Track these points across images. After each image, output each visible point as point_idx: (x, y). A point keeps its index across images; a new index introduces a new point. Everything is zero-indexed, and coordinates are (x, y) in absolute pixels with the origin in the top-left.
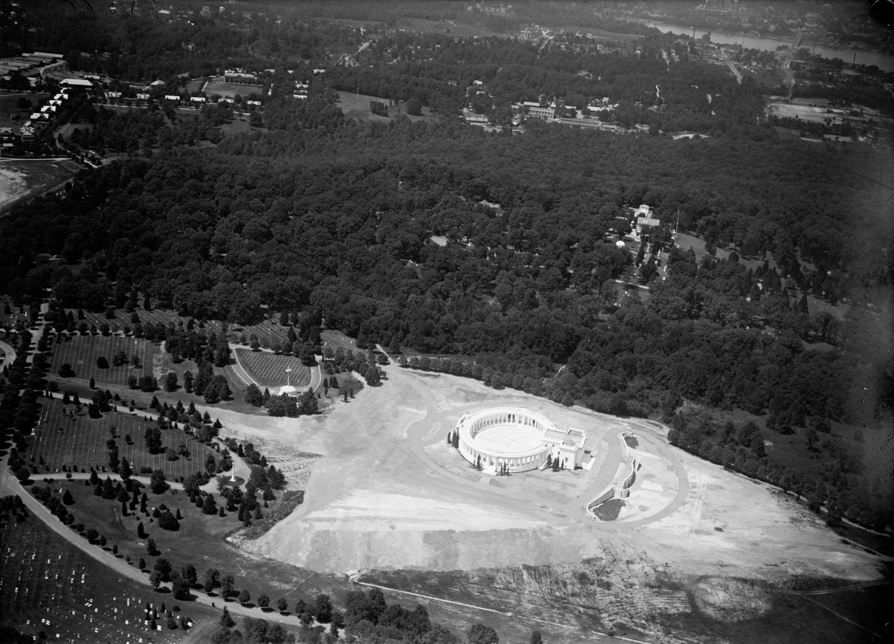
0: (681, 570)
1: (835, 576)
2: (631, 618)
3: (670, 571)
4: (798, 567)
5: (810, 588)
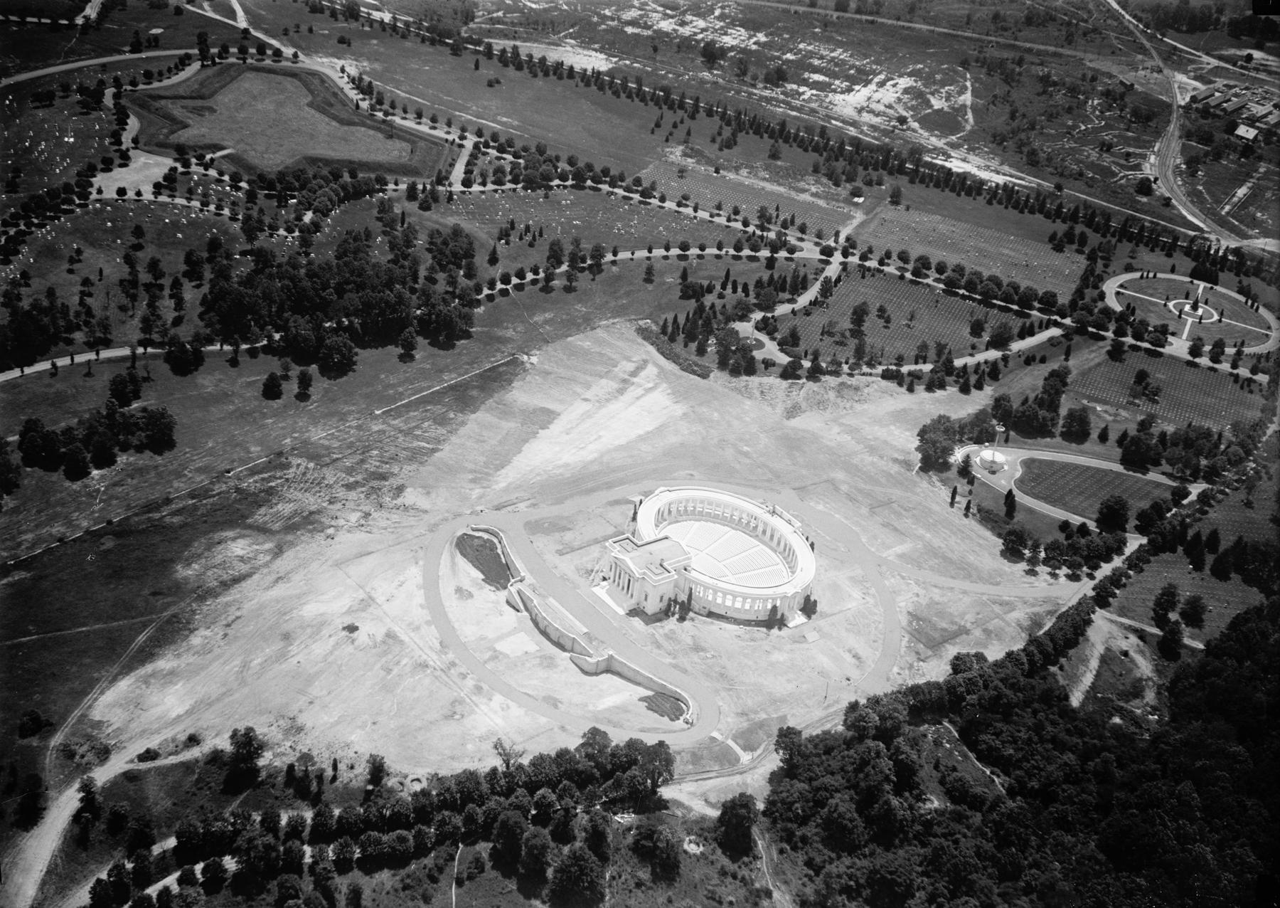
0: (306, 548)
1: (149, 668)
2: (287, 480)
3: (320, 537)
4: (204, 646)
5: (160, 629)
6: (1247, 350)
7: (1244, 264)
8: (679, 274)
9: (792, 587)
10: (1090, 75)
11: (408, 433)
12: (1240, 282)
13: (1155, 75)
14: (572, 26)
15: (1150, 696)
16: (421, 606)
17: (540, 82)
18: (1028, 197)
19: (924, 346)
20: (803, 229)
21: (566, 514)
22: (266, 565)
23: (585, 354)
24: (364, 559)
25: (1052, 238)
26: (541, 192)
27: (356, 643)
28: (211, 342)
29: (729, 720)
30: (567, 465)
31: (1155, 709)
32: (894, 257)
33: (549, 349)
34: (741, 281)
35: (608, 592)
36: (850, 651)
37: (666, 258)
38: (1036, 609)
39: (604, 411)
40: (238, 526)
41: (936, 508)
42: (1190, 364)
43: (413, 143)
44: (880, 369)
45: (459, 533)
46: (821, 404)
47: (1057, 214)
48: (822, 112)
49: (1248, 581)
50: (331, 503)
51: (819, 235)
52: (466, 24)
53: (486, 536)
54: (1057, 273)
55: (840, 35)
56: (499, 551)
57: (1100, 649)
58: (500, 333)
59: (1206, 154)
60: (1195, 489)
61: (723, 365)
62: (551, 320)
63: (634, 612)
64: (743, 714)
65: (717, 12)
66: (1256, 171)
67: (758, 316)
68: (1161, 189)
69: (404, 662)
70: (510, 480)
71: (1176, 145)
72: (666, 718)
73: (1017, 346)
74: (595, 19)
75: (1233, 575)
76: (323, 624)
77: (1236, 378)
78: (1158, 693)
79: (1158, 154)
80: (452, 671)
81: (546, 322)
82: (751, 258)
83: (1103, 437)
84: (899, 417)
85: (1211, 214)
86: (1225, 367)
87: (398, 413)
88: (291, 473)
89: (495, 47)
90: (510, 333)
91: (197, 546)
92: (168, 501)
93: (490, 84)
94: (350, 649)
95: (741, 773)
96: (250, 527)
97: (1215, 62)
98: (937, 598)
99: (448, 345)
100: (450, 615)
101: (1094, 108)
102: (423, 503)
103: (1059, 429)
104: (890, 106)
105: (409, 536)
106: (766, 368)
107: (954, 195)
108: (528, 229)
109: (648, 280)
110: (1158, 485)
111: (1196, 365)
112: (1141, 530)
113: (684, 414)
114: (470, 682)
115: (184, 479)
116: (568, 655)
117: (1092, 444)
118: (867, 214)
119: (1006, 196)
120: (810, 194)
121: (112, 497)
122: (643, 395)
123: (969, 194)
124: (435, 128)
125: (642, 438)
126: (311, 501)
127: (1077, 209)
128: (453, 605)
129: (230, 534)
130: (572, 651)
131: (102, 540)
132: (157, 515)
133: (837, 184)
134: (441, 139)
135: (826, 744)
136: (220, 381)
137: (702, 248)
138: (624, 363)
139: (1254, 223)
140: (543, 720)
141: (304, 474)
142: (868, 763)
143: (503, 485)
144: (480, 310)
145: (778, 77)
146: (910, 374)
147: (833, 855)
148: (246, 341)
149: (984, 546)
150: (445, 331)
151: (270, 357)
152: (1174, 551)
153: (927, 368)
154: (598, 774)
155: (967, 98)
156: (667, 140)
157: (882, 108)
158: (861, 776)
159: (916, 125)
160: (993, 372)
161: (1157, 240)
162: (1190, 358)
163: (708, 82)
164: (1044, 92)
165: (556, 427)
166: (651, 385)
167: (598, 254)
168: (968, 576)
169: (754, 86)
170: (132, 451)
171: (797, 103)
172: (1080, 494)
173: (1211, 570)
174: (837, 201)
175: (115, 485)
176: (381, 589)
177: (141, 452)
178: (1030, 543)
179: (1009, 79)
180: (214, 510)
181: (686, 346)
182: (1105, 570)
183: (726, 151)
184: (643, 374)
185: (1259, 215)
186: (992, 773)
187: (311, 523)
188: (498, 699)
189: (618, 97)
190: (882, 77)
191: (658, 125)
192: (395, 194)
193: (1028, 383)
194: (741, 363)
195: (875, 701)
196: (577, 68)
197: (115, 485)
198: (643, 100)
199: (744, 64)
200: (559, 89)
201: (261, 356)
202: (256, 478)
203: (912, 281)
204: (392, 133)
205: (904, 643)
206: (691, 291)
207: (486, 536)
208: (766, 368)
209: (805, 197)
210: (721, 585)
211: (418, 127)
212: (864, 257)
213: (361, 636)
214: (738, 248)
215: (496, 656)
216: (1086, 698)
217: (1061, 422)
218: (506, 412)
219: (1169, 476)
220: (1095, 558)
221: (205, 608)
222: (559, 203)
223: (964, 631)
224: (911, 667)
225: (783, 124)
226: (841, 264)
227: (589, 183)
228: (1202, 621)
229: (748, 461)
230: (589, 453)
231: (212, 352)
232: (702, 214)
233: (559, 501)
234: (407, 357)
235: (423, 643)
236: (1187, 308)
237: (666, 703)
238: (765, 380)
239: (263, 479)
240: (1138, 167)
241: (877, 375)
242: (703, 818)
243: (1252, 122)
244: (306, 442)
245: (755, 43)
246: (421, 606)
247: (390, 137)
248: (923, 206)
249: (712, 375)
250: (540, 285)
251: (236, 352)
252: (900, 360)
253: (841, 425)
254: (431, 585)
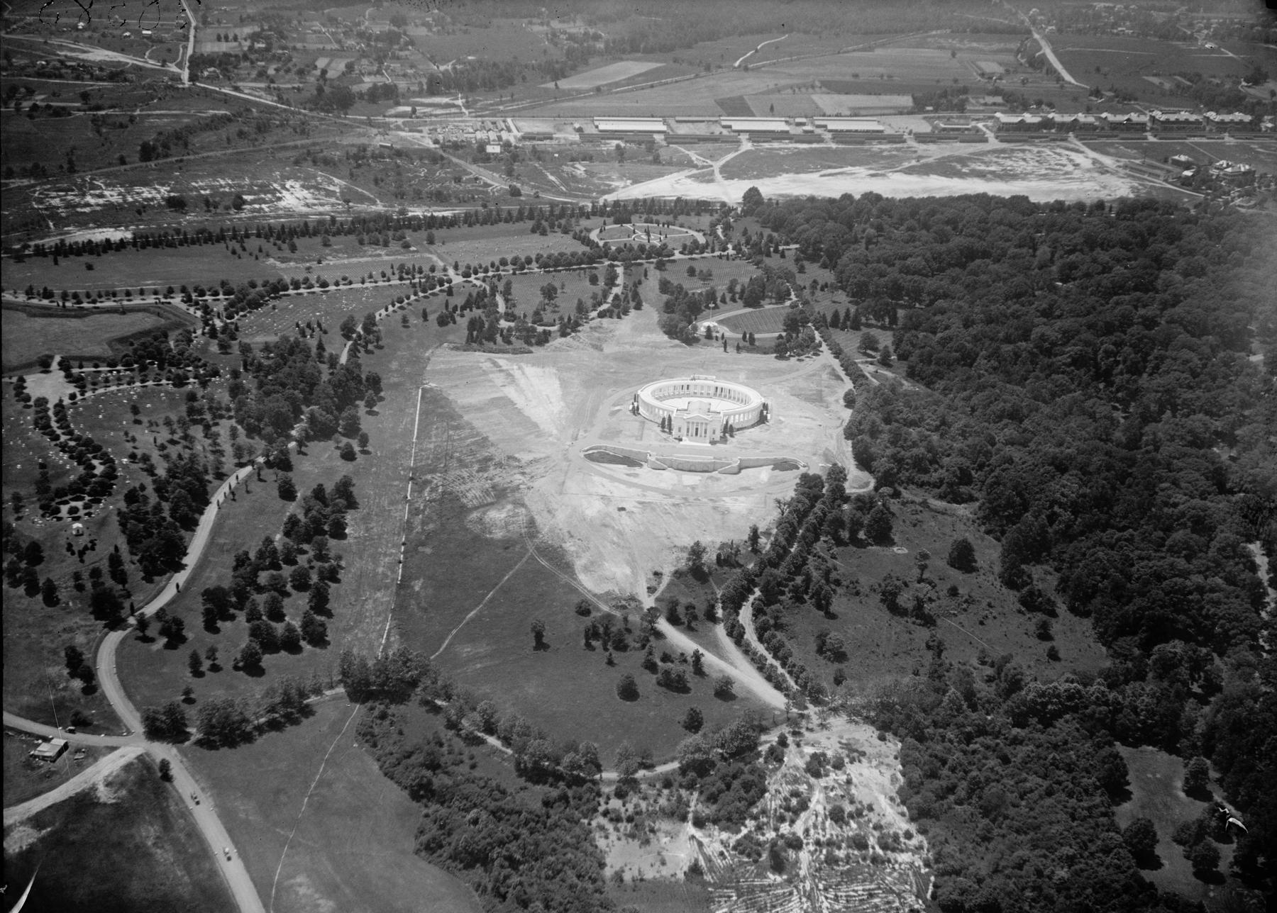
63: (713, 442)
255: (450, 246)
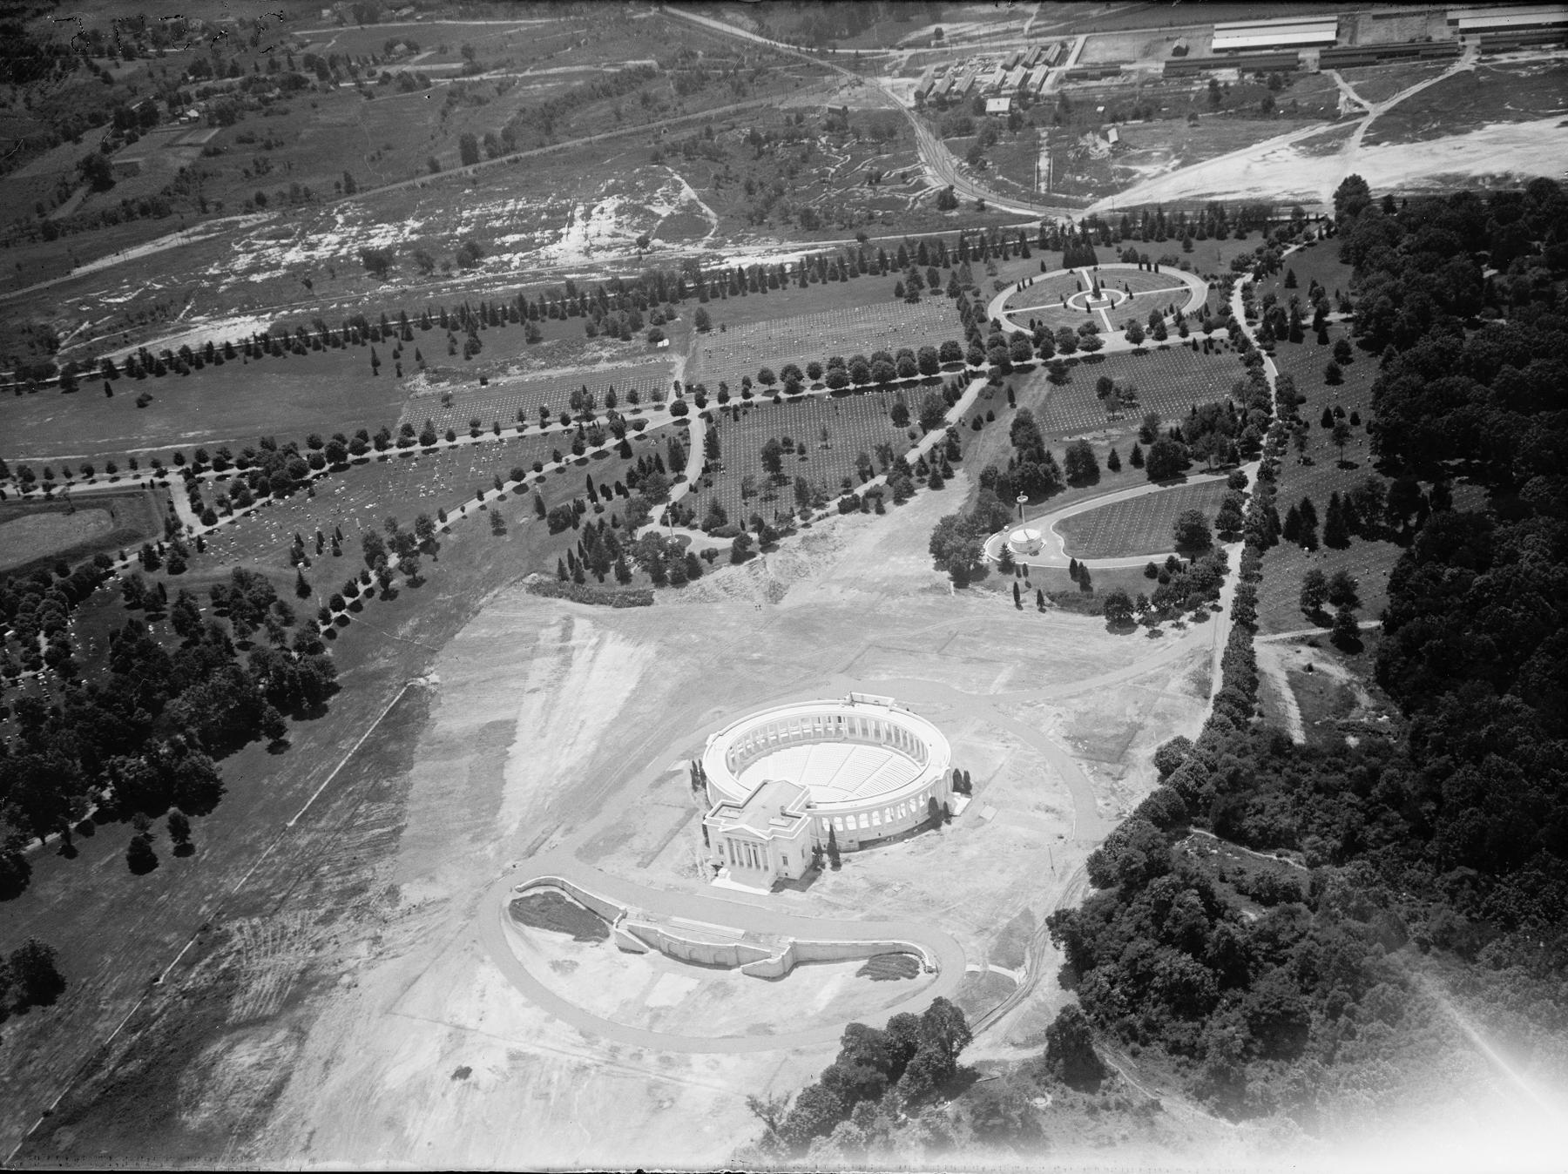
0: (329, 1019)
2: (239, 952)
3: (338, 993)
6: (1185, 311)
7: (1107, 231)
8: (531, 507)
9: (938, 768)
10: (793, 117)
11: (348, 827)
12: (1119, 250)
13: (858, 89)
14: (186, 302)
15: (1364, 699)
16: (525, 1005)
17: (197, 377)
18: (841, 261)
19: (863, 459)
20: (633, 398)
21: (614, 822)
22: (297, 1056)
23: (475, 648)
24: (416, 987)
25: (899, 293)
26: (302, 492)
27: (481, 1086)
28: (25, 841)
29: (973, 944)
30: (570, 770)
31: (1379, 710)
32: (755, 383)
33: (442, 658)
34: (610, 483)
35: (733, 878)
36: (1038, 808)
37: (502, 498)
38: (1191, 668)
39: (564, 693)
40: (221, 1033)
41: (1005, 618)
42: (1137, 352)
43: (105, 505)
44: (833, 505)
45: (507, 903)
46: (799, 571)
47: (882, 267)
48: (548, 272)
49: (1371, 534)
50: (317, 950)
51: (657, 397)
52: (52, 353)
53: (541, 891)
54: (931, 322)
55: (498, 185)
56: (569, 899)
57: (1281, 679)
58: (371, 667)
59: (981, 142)
60: (1251, 470)
61: (659, 581)
62: (420, 625)
63: (779, 885)
64: (982, 931)
65: (340, 219)
66: (1039, 138)
67: (657, 511)
68: (963, 196)
69: (555, 1077)
70: (519, 817)
71: (940, 148)
72: (903, 979)
73: (953, 415)
74: (206, 284)
75: (1351, 538)
76: (423, 1085)
77: (1195, 345)
78: (1371, 692)
79: (929, 163)
80: (620, 1058)
81: (416, 630)
82: (600, 455)
83: (1114, 465)
84: (890, 544)
85: (1033, 198)
86: (1174, 339)
87: (317, 811)
88: (237, 941)
89: (115, 362)
90: (383, 663)
91: (188, 1080)
92: (106, 1051)
93: (142, 404)
94: (479, 1097)
95: (1028, 995)
96: (237, 1026)
97: (908, 53)
98: (1082, 708)
99: (318, 711)
100: (568, 998)
101: (827, 146)
102: (435, 892)
103: (1063, 481)
104: (615, 235)
105: (449, 936)
106: (711, 561)
107: (759, 294)
108: (320, 536)
109: (499, 532)
110: (1207, 485)
111: (1144, 352)
112: (1229, 537)
113: (658, 653)
114: (651, 1059)
115: (106, 1016)
116: (738, 970)
117: (1107, 477)
118: (684, 353)
119: (814, 272)
120: (604, 361)
121: (27, 1083)
122: (595, 655)
123: (774, 286)
124: (116, 479)
125: (634, 698)
126: (292, 960)
127: (902, 250)
128: (561, 986)
129: (218, 1047)
130: (739, 964)
131: (55, 1138)
132: (102, 1075)
133: (627, 338)
134: (134, 487)
135: (1102, 914)
136: (68, 880)
137: (538, 468)
138: (544, 631)
139: (1083, 188)
140: (768, 1055)
141: (255, 935)
142: (1168, 905)
143: (515, 826)
144: (329, 652)
145: (471, 254)
146: (869, 495)
147: (1197, 1024)
148: (73, 817)
149: (1087, 633)
150: (306, 693)
151: (110, 825)
152: (1275, 543)
153: (881, 480)
154: (884, 1076)
155: (688, 192)
156: (400, 375)
157: (609, 240)
158: (1168, 923)
159: (657, 242)
160: (952, 452)
161: (1004, 245)
162: (1135, 346)
163: (394, 295)
164: (761, 153)
165: (524, 735)
166: (594, 640)
167: (425, 526)
168: (1095, 671)
169: (450, 277)
170: (13, 1016)
171: (511, 274)
172: (1140, 531)
173: (1327, 542)
174: (642, 354)
175: (20, 1066)
176: (463, 1011)
177: (27, 1012)
178: (1135, 603)
179: (714, 155)
180: (172, 1033)
181: (602, 580)
182: (1228, 592)
183: (475, 357)
184: (576, 632)
185: (1079, 178)
186: (1279, 856)
187: (313, 983)
188: (698, 1060)
189: (305, 353)
190: (580, 209)
191: (376, 363)
192: (127, 572)
193: (994, 447)
194: (681, 570)
195: (1113, 842)
196: (234, 342)
197: (20, 1066)
198: (336, 344)
199: (423, 259)
200: (227, 375)
201: (98, 829)
202: (197, 969)
203: (790, 400)
204: (70, 506)
205: (1086, 771)
206: (561, 521)
207: (541, 891)
208: (711, 561)
209: (602, 366)
210: (860, 804)
211: (93, 487)
212: (723, 398)
213: (480, 1073)
214: (578, 450)
215: (657, 1015)
216: (1307, 733)
217: (1063, 469)
218: (450, 748)
219: (1210, 471)
220: (1209, 585)
221: (260, 1145)
222: (332, 494)
223: (1135, 728)
224: (1114, 792)
225: (521, 300)
226: (702, 416)
227: (351, 457)
228: (1356, 598)
229: (768, 667)
230: (586, 745)
231: (34, 852)
232: (509, 434)
233: (595, 812)
234: (279, 747)
235: (558, 1045)
236: (1089, 299)
237: (891, 963)
238: (719, 574)
239: (208, 966)
240: (921, 185)
241: (834, 513)
242: (1026, 1066)
243: (995, 92)
244: (229, 900)
245: (412, 233)
246: (525, 1005)
247: (73, 510)
248: (738, 319)
249: (654, 596)
250: (378, 594)
251: (67, 836)
252: (847, 485)
253: (838, 581)
254: (518, 976)
255: (739, 334)
